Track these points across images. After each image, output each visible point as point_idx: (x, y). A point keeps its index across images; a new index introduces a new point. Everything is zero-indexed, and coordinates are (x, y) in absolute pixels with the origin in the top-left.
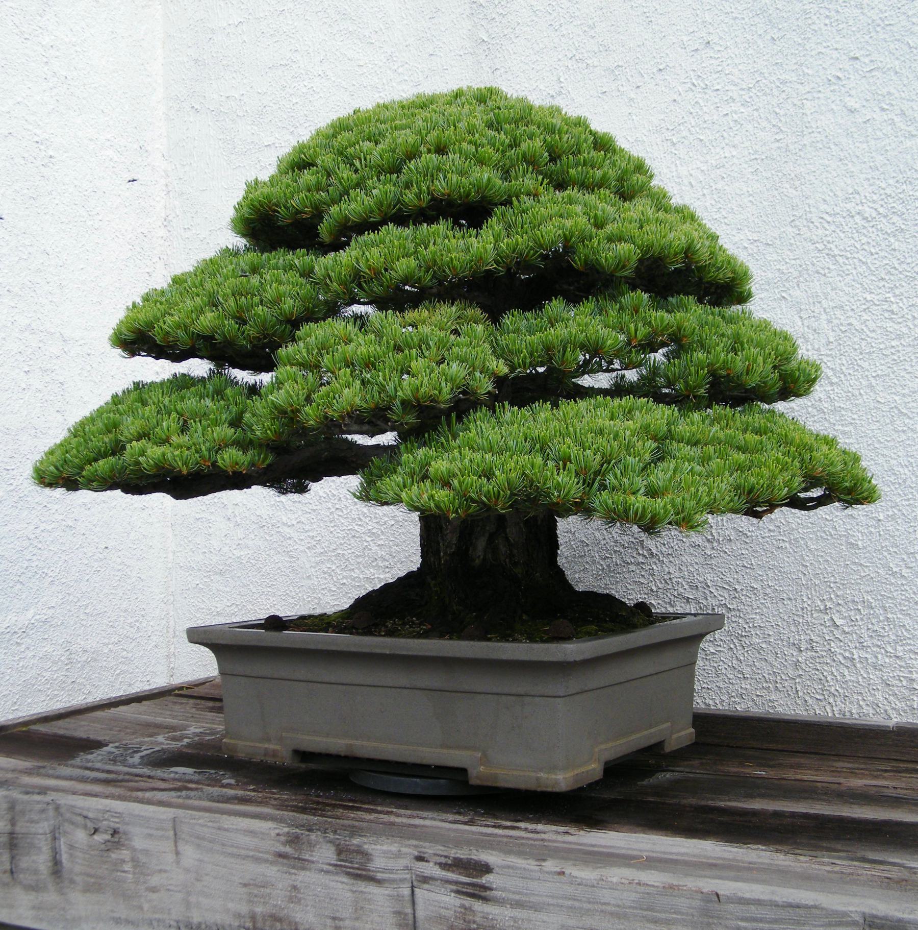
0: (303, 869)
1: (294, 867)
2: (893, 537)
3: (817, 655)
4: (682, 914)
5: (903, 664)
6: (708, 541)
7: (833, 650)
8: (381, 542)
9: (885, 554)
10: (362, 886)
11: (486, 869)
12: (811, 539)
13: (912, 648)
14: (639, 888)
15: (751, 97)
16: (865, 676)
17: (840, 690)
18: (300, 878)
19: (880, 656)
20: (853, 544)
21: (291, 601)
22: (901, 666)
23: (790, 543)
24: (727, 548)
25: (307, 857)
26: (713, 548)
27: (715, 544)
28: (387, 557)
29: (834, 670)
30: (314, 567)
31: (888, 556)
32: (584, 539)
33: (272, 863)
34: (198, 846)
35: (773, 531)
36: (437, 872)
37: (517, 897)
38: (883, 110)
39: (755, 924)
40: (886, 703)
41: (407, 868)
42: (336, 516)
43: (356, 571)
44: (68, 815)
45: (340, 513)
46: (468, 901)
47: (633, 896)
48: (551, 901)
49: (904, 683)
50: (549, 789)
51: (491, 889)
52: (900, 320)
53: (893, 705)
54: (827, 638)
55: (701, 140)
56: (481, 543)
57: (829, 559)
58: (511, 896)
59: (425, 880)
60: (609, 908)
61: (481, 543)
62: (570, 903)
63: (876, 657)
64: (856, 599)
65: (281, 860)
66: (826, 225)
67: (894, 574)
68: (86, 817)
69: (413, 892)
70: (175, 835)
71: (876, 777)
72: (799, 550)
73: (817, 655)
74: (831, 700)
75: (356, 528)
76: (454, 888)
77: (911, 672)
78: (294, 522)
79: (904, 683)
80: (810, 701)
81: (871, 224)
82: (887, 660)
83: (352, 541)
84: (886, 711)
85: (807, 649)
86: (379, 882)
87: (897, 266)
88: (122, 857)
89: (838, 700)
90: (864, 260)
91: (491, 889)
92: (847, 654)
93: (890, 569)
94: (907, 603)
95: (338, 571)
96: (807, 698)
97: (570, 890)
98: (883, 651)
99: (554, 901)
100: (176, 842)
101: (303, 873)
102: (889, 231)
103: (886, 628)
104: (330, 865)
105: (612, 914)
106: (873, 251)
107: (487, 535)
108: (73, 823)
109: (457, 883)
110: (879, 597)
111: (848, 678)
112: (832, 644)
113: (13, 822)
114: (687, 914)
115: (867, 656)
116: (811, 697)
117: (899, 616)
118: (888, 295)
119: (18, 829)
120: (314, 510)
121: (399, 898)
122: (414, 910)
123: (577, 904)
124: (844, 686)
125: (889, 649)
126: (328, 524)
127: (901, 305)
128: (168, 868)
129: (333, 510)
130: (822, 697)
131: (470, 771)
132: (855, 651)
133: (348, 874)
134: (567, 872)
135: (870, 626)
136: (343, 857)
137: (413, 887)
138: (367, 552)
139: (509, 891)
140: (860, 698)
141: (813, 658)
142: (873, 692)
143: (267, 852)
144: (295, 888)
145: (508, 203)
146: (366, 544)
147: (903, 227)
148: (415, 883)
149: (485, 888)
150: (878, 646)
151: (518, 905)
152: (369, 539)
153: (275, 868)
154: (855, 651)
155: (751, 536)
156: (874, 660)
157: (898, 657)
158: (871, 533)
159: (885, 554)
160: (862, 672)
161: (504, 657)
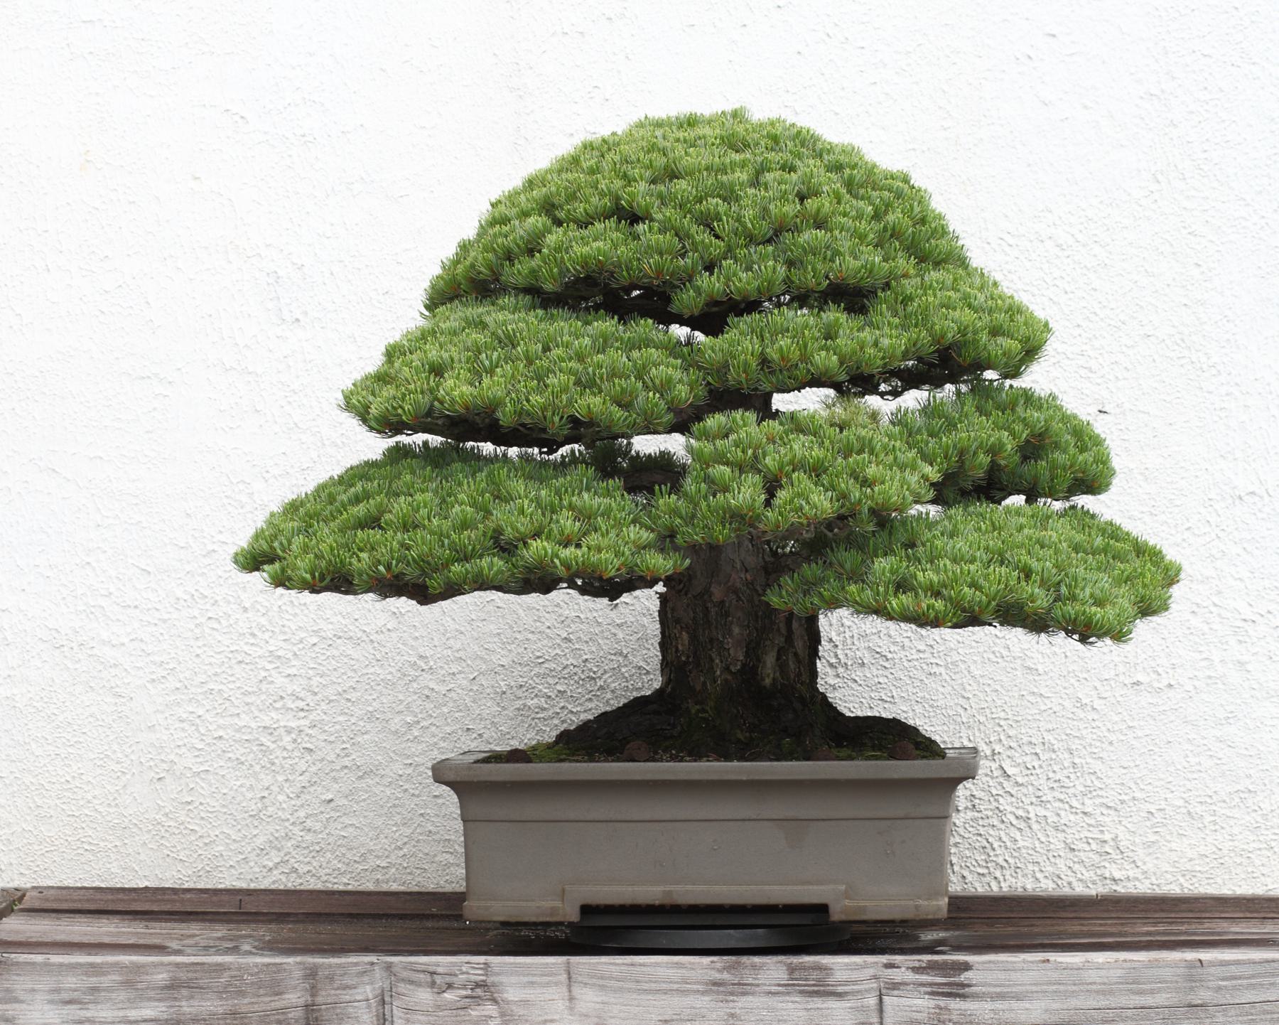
0: (744, 994)
1: (732, 994)
2: (1082, 659)
3: (979, 815)
4: (1166, 982)
5: (1092, 822)
6: (831, 665)
7: (1002, 808)
8: (293, 671)
9: (1072, 681)
10: (818, 1003)
11: (966, 967)
12: (975, 662)
13: (1104, 801)
14: (1125, 965)
15: (909, 65)
16: (1043, 839)
17: (1010, 860)
18: (740, 1005)
19: (1063, 813)
20: (1030, 669)
21: (117, 767)
22: (1089, 825)
23: (947, 667)
24: (858, 674)
25: (750, 981)
26: (838, 676)
27: (841, 670)
28: (302, 695)
29: (1002, 834)
30: (163, 712)
31: (1076, 684)
32: (641, 664)
33: (704, 993)
34: (602, 987)
35: (924, 652)
36: (911, 976)
37: (998, 990)
38: (1086, 107)
39: (1234, 982)
40: (1069, 873)
41: (875, 977)
42: (207, 630)
43: (243, 716)
44: (405, 974)
45: (216, 626)
46: (942, 1002)
47: (1119, 972)
48: (1034, 988)
49: (1094, 846)
50: (930, 917)
51: (969, 986)
52: (1099, 381)
53: (1079, 876)
54: (994, 792)
55: (837, 114)
56: (770, 659)
57: (998, 688)
58: (992, 990)
59: (895, 986)
60: (1094, 987)
61: (770, 659)
62: (1054, 987)
63: (1058, 815)
64: (1034, 740)
65: (715, 988)
66: (1007, 249)
67: (1083, 706)
68: (433, 973)
69: (881, 1000)
70: (569, 978)
71: (1155, 924)
72: (957, 676)
73: (979, 815)
74: (998, 874)
75: (246, 648)
76: (929, 990)
77: (1102, 832)
78: (126, 640)
79: (1094, 846)
80: (969, 878)
81: (1066, 253)
82: (1072, 817)
83: (237, 669)
84: (1070, 883)
85: (966, 808)
86: (840, 995)
87: (1098, 312)
88: (486, 1013)
89: (1007, 873)
90: (1055, 299)
91: (969, 986)
92: (1020, 813)
93: (1079, 700)
94: (1098, 744)
95: (208, 716)
96: (966, 873)
97: (1055, 975)
98: (1067, 807)
99: (1038, 988)
100: (569, 986)
101: (744, 999)
102: (1089, 266)
103: (1072, 776)
104: (779, 985)
105: (1097, 992)
106: (1068, 289)
107: (776, 649)
108: (412, 982)
109: (931, 985)
110: (1064, 737)
111: (1021, 844)
112: (1001, 800)
113: (314, 991)
114: (1171, 982)
115: (1048, 814)
116: (971, 872)
117: (1089, 760)
118: (1084, 347)
119: (319, 1000)
120: (165, 621)
121: (862, 1009)
122: (881, 1018)
123: (1062, 988)
124: (1015, 854)
125: (1075, 803)
126: (192, 642)
127: (1101, 360)
128: (556, 1017)
129: (203, 620)
130: (985, 871)
131: (831, 910)
132: (1030, 808)
133: (801, 992)
134: (1052, 959)
135: (1051, 775)
136: (796, 975)
137: (880, 996)
138: (264, 686)
139: (990, 985)
140: (1036, 869)
141: (974, 820)
142: (1053, 860)
143: (698, 983)
144: (732, 1015)
145: (887, 286)
146: (264, 674)
147: (1107, 261)
148: (884, 991)
149: (963, 985)
150: (1061, 801)
151: (1001, 996)
152: (269, 666)
153: (707, 998)
154: (1030, 808)
155: (893, 659)
156: (1056, 819)
157: (1085, 813)
158: (1055, 653)
159: (1072, 681)
160: (1040, 835)
161: (896, 776)
